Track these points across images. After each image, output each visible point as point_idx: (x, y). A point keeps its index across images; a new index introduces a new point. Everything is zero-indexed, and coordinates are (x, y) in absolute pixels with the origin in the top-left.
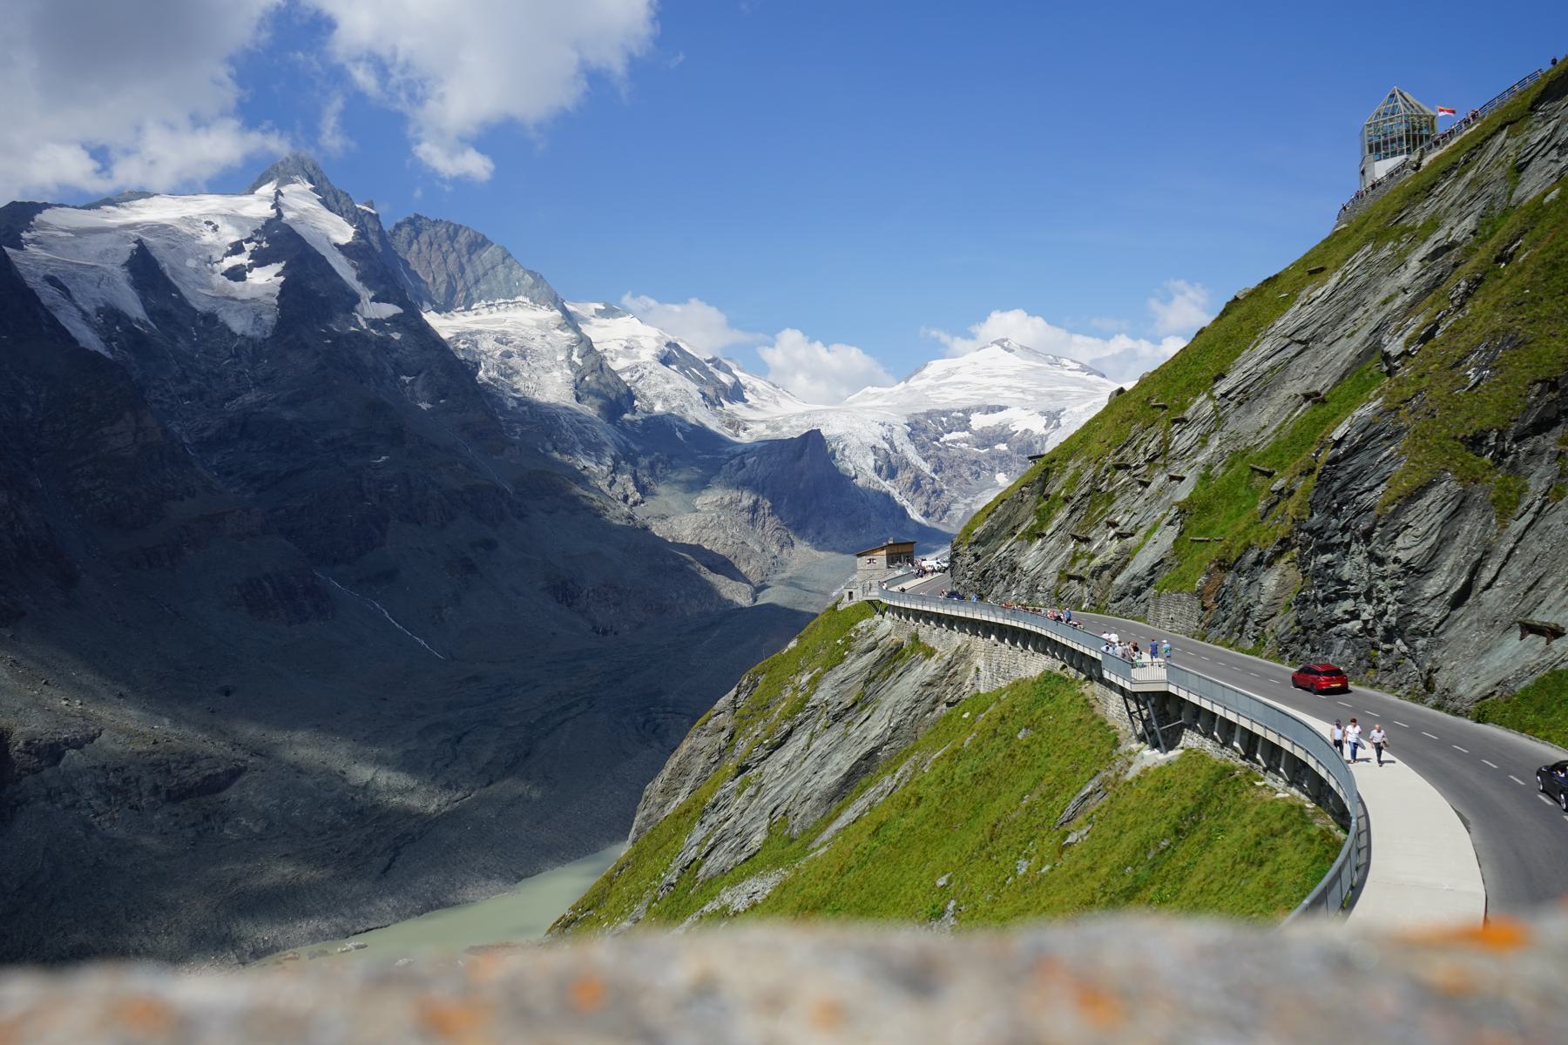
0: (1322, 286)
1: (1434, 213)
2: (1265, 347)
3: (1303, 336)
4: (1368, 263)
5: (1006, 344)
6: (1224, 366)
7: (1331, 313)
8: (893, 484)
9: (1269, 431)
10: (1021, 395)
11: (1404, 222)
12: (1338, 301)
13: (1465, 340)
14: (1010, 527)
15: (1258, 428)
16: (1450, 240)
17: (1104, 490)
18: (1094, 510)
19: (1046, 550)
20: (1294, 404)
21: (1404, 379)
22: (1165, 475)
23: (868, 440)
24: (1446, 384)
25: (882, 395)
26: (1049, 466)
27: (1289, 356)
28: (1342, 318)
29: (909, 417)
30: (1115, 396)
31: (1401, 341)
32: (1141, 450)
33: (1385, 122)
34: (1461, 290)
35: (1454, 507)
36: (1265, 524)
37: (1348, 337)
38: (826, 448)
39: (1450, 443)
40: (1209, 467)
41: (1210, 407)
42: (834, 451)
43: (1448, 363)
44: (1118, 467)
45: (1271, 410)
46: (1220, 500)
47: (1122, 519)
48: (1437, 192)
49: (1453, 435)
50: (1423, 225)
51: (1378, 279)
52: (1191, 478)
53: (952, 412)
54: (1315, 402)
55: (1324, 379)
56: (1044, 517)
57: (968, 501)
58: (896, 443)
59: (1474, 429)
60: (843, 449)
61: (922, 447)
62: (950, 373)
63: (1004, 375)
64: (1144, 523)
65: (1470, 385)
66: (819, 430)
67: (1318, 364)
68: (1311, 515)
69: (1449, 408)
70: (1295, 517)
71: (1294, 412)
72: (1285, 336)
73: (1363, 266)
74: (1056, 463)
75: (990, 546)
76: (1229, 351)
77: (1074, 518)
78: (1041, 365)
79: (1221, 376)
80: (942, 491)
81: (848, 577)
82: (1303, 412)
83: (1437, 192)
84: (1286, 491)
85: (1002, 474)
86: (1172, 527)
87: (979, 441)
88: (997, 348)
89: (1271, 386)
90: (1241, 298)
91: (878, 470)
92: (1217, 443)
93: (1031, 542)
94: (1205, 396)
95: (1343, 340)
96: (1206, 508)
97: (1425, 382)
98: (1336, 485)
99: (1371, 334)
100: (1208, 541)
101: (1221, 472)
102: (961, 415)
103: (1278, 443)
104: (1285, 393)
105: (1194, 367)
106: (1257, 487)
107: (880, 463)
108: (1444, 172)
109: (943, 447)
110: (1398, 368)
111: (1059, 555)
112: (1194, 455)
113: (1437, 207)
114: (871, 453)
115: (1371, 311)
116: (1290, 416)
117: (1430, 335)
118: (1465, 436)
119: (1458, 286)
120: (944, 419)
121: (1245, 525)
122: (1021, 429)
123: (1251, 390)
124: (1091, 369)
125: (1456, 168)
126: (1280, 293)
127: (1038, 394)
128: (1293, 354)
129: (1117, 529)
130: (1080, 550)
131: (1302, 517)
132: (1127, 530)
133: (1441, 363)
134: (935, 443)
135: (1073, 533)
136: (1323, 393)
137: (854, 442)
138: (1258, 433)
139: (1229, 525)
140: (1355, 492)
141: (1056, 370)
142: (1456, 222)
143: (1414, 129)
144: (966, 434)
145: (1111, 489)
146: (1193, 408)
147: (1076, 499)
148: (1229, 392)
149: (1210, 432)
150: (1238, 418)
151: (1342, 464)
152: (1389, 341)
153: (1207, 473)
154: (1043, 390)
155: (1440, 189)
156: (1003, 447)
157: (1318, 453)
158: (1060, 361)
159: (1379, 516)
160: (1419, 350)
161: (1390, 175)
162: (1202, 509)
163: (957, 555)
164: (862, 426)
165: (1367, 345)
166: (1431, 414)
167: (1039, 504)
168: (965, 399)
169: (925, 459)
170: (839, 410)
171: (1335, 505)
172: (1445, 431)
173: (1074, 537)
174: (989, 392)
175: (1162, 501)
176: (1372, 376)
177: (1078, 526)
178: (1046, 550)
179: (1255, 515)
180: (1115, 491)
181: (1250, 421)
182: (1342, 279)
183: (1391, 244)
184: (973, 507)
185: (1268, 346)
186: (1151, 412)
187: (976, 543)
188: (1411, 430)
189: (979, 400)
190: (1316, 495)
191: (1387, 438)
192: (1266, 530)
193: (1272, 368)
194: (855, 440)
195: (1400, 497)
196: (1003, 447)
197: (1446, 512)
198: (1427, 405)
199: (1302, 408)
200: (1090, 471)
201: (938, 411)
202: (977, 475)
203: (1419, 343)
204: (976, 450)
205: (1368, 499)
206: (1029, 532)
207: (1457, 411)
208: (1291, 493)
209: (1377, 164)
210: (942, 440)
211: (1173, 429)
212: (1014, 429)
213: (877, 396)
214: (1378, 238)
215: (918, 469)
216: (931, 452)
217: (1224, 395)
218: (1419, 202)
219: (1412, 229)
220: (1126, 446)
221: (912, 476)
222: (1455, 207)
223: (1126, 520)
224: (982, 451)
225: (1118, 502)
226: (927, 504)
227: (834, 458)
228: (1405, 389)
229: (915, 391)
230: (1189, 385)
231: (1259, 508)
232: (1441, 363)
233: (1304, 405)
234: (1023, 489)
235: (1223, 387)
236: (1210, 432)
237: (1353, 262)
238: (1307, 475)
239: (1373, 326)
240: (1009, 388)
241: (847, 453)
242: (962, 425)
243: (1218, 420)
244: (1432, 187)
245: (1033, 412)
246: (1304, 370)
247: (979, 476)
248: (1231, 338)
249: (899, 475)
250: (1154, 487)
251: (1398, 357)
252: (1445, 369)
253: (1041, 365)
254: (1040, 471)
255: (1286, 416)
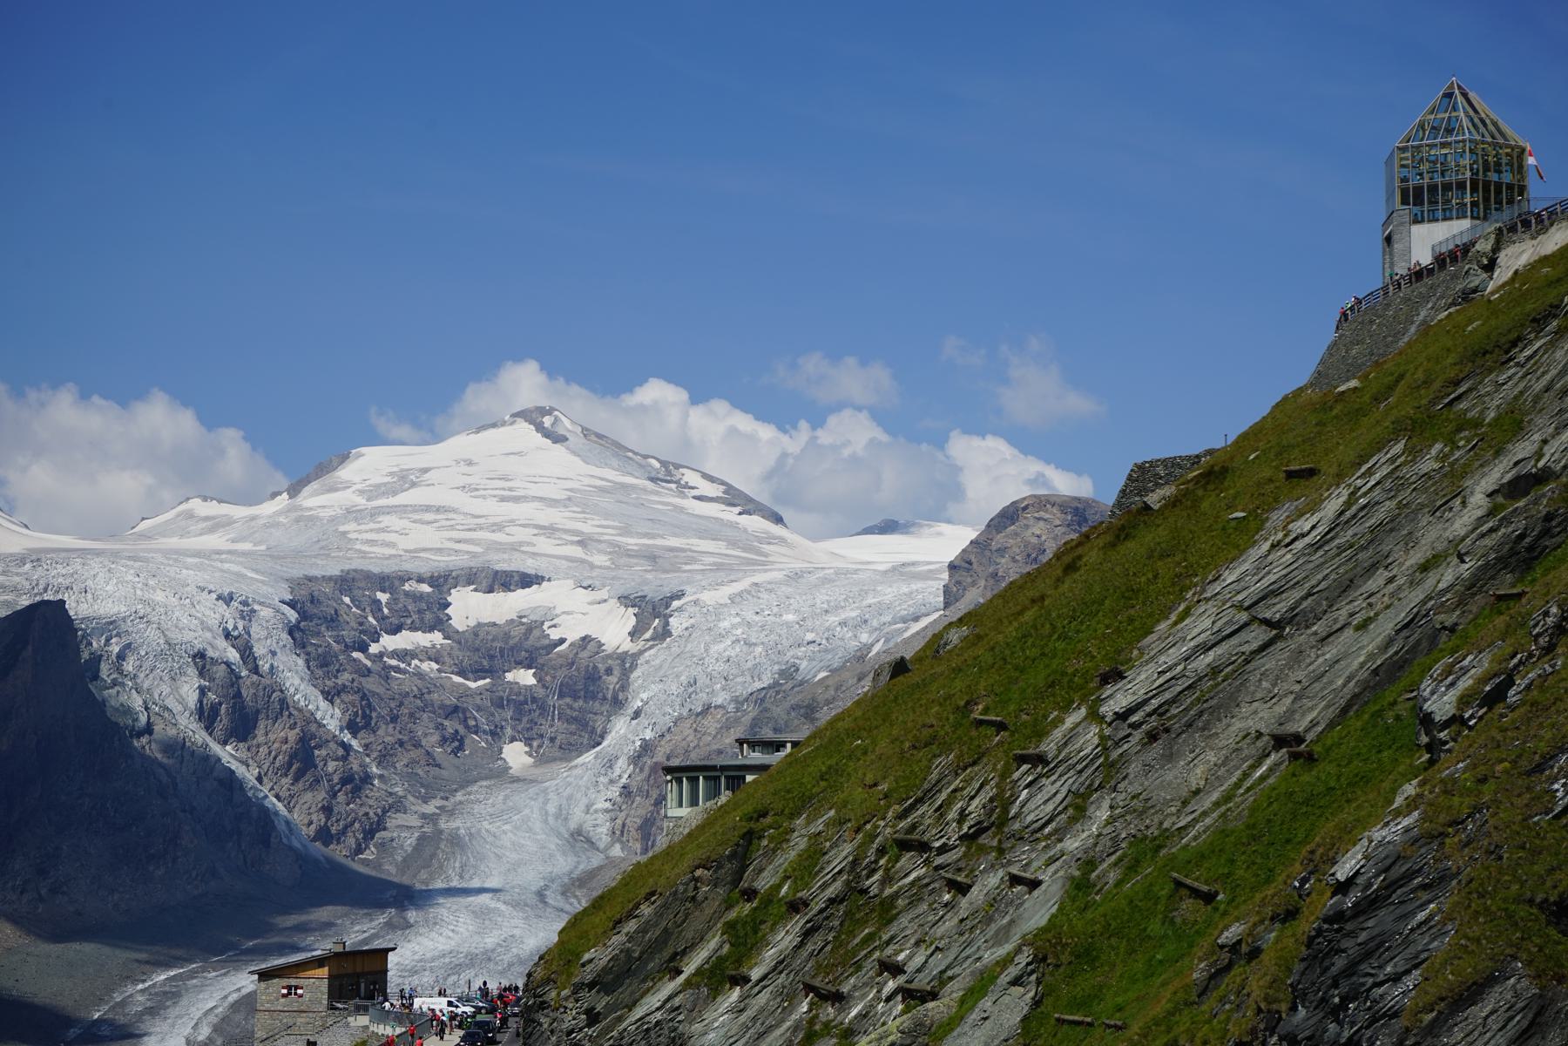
0: (1313, 511)
1: (1516, 398)
2: (1201, 625)
3: (1277, 610)
4: (1396, 482)
5: (547, 421)
6: (1119, 652)
7: (1327, 573)
8: (243, 754)
9: (1207, 803)
10: (577, 552)
11: (1463, 405)
12: (1341, 549)
13: (1553, 726)
14: (666, 954)
15: (1184, 793)
16: (1540, 464)
17: (874, 891)
18: (852, 934)
19: (749, 1013)
20: (1251, 751)
21: (1455, 781)
22: (1001, 873)
23: (188, 636)
24: (1518, 802)
25: (228, 522)
26: (752, 825)
27: (1247, 648)
28: (1347, 586)
29: (295, 584)
30: (885, 677)
31: (1451, 697)
32: (952, 815)
33: (1432, 146)
34: (1550, 620)
35: (1525, 1023)
36: (1204, 1007)
37: (1359, 628)
38: (78, 652)
39: (1522, 911)
40: (1089, 864)
41: (1090, 737)
42: (96, 659)
43: (1524, 764)
44: (904, 846)
45: (1211, 757)
46: (1113, 941)
47: (910, 957)
48: (1522, 358)
49: (1529, 895)
50: (1497, 419)
51: (1413, 516)
52: (1053, 883)
53: (404, 579)
54: (1294, 756)
55: (1312, 709)
56: (745, 939)
57: (430, 808)
58: (259, 650)
59: (1561, 889)
60: (121, 657)
61: (321, 664)
62: (404, 480)
63: (541, 499)
64: (956, 970)
65: (1558, 809)
66: (62, 602)
67: (1300, 675)
68: (1294, 1009)
69: (1523, 848)
70: (1263, 1006)
71: (1254, 767)
72: (1240, 607)
73: (1388, 485)
74: (768, 820)
75: (623, 994)
76: (1131, 620)
77: (810, 947)
78: (629, 480)
79: (1115, 675)
80: (367, 779)
81: (110, 990)
82: (1271, 770)
83: (1522, 358)
84: (1244, 948)
85: (519, 747)
86: (1019, 990)
87: (467, 659)
88: (524, 429)
89: (1213, 710)
90: (1156, 507)
91: (207, 715)
92: (1103, 814)
93: (715, 992)
94: (1083, 711)
95: (1349, 632)
96: (1087, 955)
97: (1487, 794)
98: (1340, 962)
99: (1398, 632)
100: (1090, 1025)
101: (1113, 877)
102: (426, 588)
103: (1224, 833)
104: (1238, 725)
105: (1060, 645)
106: (1184, 922)
107: (212, 696)
108: (1534, 320)
109: (376, 667)
110: (1446, 743)
111: (777, 1025)
112: (1059, 833)
113: (1521, 386)
114: (192, 671)
115: (1401, 581)
116: (1246, 775)
117: (1495, 698)
118: (1546, 900)
119: (1546, 614)
120: (383, 597)
121: (1169, 1006)
122: (573, 635)
123: (1174, 711)
124: (750, 500)
125: (1555, 316)
126: (1231, 507)
127: (618, 551)
128: (1255, 645)
129: (901, 979)
130: (823, 1018)
131: (1275, 1007)
132: (922, 982)
133: (1514, 762)
134: (355, 655)
135: (807, 979)
136: (1310, 737)
137: (150, 638)
138: (1185, 803)
139: (1131, 995)
140: (1371, 980)
141: (666, 497)
142: (1551, 430)
143: (1486, 169)
144: (437, 638)
145: (888, 891)
146: (1058, 734)
147: (816, 907)
148: (1130, 711)
149: (1091, 790)
150: (1148, 768)
151: (1349, 926)
152: (1433, 693)
153: (1086, 875)
154: (632, 542)
155: (1527, 353)
156: (526, 677)
157: (1304, 881)
158: (677, 474)
159: (1407, 1030)
160: (1481, 718)
161: (1441, 261)
162: (1078, 957)
163: (543, 1006)
164: (174, 601)
165: (1391, 652)
166: (1494, 852)
167: (729, 907)
168: (439, 551)
169: (329, 696)
170: (115, 556)
171: (1337, 1000)
172: (1515, 887)
173: (809, 988)
174: (499, 537)
175: (994, 927)
176: (1398, 718)
177: (819, 966)
178: (749, 1013)
179: (1186, 988)
180: (896, 895)
181: (1169, 776)
182: (1348, 504)
183: (1438, 446)
184: (443, 825)
185: (1207, 623)
186: (974, 733)
187: (591, 986)
188: (1463, 877)
189: (474, 555)
190: (1303, 973)
191: (1424, 887)
192: (1209, 1022)
193: (1214, 670)
194: (152, 633)
195: (1442, 999)
196: (526, 677)
197: (1512, 1029)
198: (1489, 834)
199: (1268, 762)
200: (847, 848)
201: (368, 576)
202: (456, 743)
203: (1481, 706)
204: (457, 679)
205: (1394, 995)
206: (712, 971)
207: (1536, 852)
208: (1255, 953)
209: (1415, 229)
210: (374, 649)
211: (1016, 775)
212: (555, 635)
213: (216, 524)
214: (1417, 430)
215: (310, 719)
216: (345, 678)
217: (1122, 716)
218: (1490, 371)
219: (1477, 424)
220: (920, 801)
221: (293, 735)
222: (1552, 393)
223: (919, 960)
224: (472, 685)
225: (904, 920)
226: (327, 810)
227: (96, 677)
228: (1456, 800)
229: (312, 519)
230: (1052, 685)
231: (1195, 976)
232: (1514, 762)
233: (1273, 757)
234: (698, 873)
235: (1118, 699)
236: (1091, 790)
237: (1370, 472)
238: (1284, 921)
239: (1402, 616)
240: (550, 530)
241: (129, 666)
242: (428, 616)
243: (1109, 770)
244: (1514, 344)
245: (603, 594)
246: (1274, 685)
247: (461, 748)
248: (1136, 592)
249: (260, 732)
250: (977, 894)
251: (1446, 724)
252: (1520, 774)
253: (629, 480)
254: (735, 837)
255: (1238, 773)
